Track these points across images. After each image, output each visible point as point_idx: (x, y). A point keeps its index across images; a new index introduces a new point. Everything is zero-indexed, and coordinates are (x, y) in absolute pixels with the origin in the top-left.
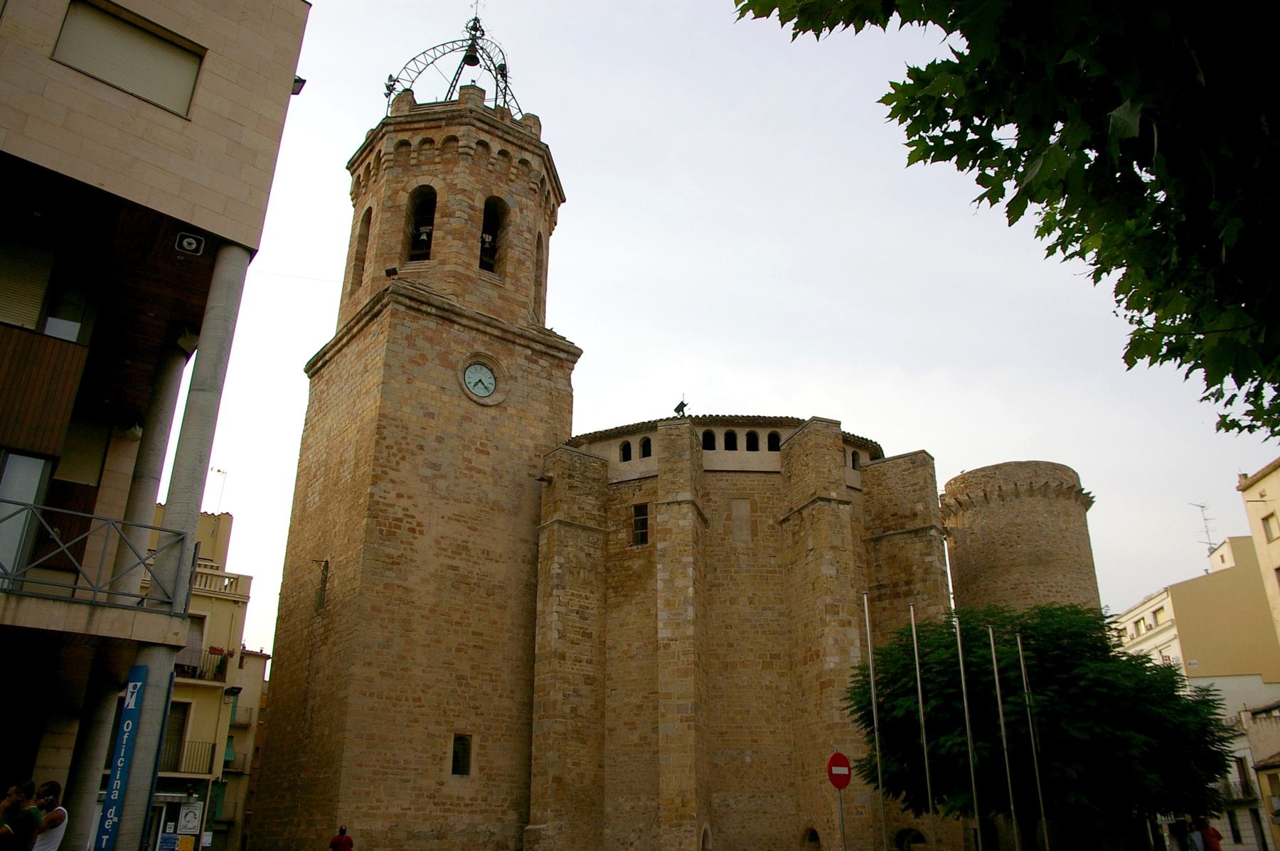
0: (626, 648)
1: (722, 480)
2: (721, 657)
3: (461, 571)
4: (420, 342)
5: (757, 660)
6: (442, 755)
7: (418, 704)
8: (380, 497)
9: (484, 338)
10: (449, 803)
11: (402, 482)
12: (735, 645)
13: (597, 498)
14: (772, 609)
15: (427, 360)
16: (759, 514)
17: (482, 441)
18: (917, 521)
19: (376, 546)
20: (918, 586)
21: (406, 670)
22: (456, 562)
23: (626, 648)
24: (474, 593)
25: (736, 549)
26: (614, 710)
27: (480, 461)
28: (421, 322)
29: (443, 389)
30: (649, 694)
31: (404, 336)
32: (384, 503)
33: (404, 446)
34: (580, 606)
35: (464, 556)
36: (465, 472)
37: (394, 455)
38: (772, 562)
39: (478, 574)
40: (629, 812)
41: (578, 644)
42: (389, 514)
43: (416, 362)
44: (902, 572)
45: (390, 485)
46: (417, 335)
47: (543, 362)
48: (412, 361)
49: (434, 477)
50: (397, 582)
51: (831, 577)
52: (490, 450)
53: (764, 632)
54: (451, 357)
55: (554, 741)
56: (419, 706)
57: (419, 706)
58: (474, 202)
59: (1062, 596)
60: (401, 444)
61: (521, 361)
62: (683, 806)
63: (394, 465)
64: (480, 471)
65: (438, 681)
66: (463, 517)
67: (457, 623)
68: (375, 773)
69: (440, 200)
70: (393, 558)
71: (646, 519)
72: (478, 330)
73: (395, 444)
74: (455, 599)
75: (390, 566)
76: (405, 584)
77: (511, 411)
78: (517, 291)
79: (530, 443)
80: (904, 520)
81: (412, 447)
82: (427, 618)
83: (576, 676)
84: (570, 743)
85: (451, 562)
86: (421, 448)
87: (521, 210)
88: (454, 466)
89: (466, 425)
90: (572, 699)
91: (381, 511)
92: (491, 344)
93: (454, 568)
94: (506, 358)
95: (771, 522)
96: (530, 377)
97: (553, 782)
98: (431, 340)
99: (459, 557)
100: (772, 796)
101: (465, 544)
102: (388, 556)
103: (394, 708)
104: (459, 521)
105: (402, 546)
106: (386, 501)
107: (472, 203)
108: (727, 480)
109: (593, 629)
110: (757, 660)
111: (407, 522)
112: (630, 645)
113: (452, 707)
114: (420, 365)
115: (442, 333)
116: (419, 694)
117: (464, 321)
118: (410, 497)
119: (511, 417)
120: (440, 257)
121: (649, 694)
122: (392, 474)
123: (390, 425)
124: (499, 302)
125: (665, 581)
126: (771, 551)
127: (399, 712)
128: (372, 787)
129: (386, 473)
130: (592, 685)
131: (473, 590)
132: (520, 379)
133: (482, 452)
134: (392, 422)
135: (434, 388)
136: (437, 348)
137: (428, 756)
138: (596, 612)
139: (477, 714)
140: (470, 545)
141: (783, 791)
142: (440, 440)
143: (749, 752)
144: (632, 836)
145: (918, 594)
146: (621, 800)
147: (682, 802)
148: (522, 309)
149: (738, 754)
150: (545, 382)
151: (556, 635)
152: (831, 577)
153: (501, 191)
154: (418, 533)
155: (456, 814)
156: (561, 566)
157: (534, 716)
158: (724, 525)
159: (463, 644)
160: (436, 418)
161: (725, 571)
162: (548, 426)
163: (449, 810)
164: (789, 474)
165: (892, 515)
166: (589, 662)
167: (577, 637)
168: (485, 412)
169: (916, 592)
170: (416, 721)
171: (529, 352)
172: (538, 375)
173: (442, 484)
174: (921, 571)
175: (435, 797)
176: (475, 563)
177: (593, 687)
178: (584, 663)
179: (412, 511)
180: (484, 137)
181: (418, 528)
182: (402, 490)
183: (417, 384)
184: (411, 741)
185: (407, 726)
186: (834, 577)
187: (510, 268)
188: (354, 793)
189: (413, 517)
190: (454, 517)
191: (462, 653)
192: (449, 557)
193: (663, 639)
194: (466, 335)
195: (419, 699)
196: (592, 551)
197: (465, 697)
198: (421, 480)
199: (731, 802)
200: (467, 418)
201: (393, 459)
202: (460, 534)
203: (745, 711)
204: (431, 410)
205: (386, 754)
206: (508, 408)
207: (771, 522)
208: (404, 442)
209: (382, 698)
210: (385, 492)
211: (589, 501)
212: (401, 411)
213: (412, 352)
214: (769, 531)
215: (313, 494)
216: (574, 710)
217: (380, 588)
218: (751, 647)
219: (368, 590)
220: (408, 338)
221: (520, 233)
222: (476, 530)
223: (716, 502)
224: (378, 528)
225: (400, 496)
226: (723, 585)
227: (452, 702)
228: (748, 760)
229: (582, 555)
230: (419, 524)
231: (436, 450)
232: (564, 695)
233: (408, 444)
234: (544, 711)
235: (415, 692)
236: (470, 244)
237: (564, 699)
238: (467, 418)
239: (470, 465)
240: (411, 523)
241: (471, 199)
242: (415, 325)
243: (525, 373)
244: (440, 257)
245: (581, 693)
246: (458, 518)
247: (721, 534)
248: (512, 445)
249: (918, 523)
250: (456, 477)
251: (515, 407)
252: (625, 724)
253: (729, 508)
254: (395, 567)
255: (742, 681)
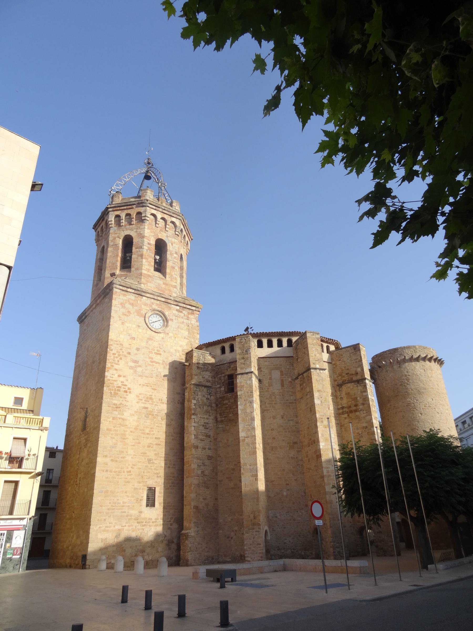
0: (226, 441)
1: (267, 361)
2: (270, 444)
3: (149, 410)
4: (127, 305)
5: (287, 445)
6: (141, 498)
7: (129, 474)
8: (110, 377)
9: (157, 303)
10: (145, 522)
11: (120, 370)
12: (276, 438)
13: (211, 372)
14: (292, 420)
15: (131, 314)
16: (284, 376)
17: (158, 349)
18: (358, 376)
19: (108, 400)
20: (361, 407)
21: (123, 458)
22: (146, 406)
23: (226, 441)
24: (155, 419)
25: (274, 393)
26: (222, 472)
27: (157, 358)
28: (128, 297)
29: (139, 326)
30: (237, 463)
31: (120, 303)
32: (112, 380)
33: (121, 353)
34: (205, 423)
35: (150, 402)
36: (150, 363)
37: (117, 357)
38: (292, 398)
39: (157, 410)
40: (230, 522)
41: (204, 441)
42: (114, 385)
43: (125, 315)
44: (353, 400)
45: (115, 372)
46: (126, 303)
47: (184, 312)
48: (124, 314)
49: (136, 367)
50: (119, 416)
51: (318, 405)
52: (161, 353)
53: (289, 432)
54: (142, 312)
55: (194, 488)
56: (130, 475)
57: (130, 475)
58: (150, 241)
59: (432, 409)
60: (120, 352)
61: (175, 312)
62: (254, 519)
63: (116, 362)
64: (157, 363)
65: (139, 462)
66: (150, 384)
67: (148, 434)
68: (108, 509)
69: (135, 241)
70: (117, 405)
71: (233, 381)
72: (154, 299)
73: (117, 352)
74: (147, 422)
75: (116, 409)
76: (123, 417)
77: (171, 334)
78: (171, 280)
79: (180, 349)
80: (351, 377)
81: (125, 353)
82: (133, 432)
83: (203, 456)
84: (201, 489)
85: (143, 405)
86: (129, 353)
87: (172, 244)
88: (145, 361)
89: (150, 342)
90: (202, 467)
91: (111, 383)
92: (161, 305)
93: (146, 408)
94: (167, 311)
95: (290, 379)
96: (179, 319)
97: (194, 508)
98: (132, 305)
99: (148, 403)
100: (298, 511)
101: (151, 396)
102: (114, 404)
103: (118, 477)
104: (148, 386)
105: (121, 399)
106: (113, 379)
107: (149, 242)
108: (269, 361)
109: (212, 433)
110: (287, 445)
111: (123, 388)
112: (228, 440)
113: (145, 474)
114: (127, 316)
115: (137, 301)
116: (130, 469)
117: (148, 295)
118: (124, 377)
119: (171, 337)
120: (136, 267)
121: (237, 463)
122: (116, 366)
123: (114, 344)
124: (163, 286)
125: (242, 410)
126: (290, 393)
127: (120, 478)
128: (107, 516)
129: (113, 366)
130: (211, 460)
131: (155, 418)
132: (174, 320)
133: (158, 354)
134: (115, 342)
135: (134, 326)
136: (136, 308)
137: (134, 499)
138: (212, 425)
139: (157, 477)
140: (153, 397)
141: (302, 509)
142: (138, 349)
143: (285, 490)
144: (232, 534)
145: (361, 410)
146: (226, 516)
147: (254, 516)
148: (174, 288)
149: (280, 491)
150: (185, 321)
151: (193, 437)
152: (318, 405)
153: (163, 236)
154: (128, 392)
155: (148, 527)
156: (195, 404)
157: (185, 477)
158: (268, 382)
159: (151, 443)
160: (136, 340)
161: (270, 403)
162: (188, 340)
163: (144, 525)
164: (297, 357)
165: (347, 374)
166: (209, 449)
167: (203, 437)
168: (159, 336)
169: (360, 410)
170: (128, 482)
171: (178, 308)
172: (182, 318)
173: (139, 369)
174: (361, 399)
175: (138, 519)
176: (156, 405)
177: (211, 461)
178: (207, 450)
179: (126, 383)
180: (118, 213)
181: (129, 391)
182: (120, 373)
183: (127, 325)
184: (126, 492)
185: (124, 485)
186: (320, 404)
187: (168, 271)
188: (98, 520)
189: (126, 385)
190: (145, 384)
191: (150, 448)
192: (143, 403)
193: (242, 437)
194: (149, 301)
195: (130, 472)
196: (209, 397)
197: (152, 469)
198: (130, 368)
199: (278, 515)
200: (150, 339)
201: (116, 359)
202: (149, 392)
203: (283, 470)
204: (133, 336)
205: (114, 500)
206: (169, 333)
207: (290, 379)
208: (121, 351)
209: (112, 472)
210: (112, 375)
211: (207, 374)
212: (120, 337)
213: (124, 310)
214: (289, 384)
215: (81, 376)
216: (203, 472)
217: (111, 419)
218: (283, 439)
219: (105, 421)
220: (121, 304)
221: (171, 254)
222: (155, 389)
223: (264, 372)
224: (110, 391)
225: (119, 376)
226: (269, 410)
227: (146, 471)
228: (285, 494)
229: (204, 399)
230: (129, 389)
231: (136, 354)
232: (198, 465)
233: (123, 352)
234: (189, 474)
235: (127, 468)
236: (149, 260)
237: (198, 468)
238: (150, 339)
239: (152, 360)
240: (125, 388)
241: (149, 240)
242: (125, 298)
243: (177, 317)
244: (136, 267)
245: (206, 464)
246: (147, 385)
247: (267, 386)
248: (171, 350)
249: (359, 377)
250: (146, 366)
251: (172, 333)
252: (227, 478)
253: (270, 374)
254: (118, 409)
255: (280, 455)
